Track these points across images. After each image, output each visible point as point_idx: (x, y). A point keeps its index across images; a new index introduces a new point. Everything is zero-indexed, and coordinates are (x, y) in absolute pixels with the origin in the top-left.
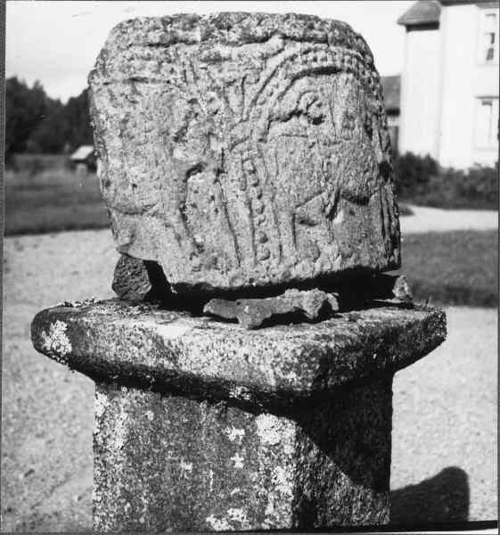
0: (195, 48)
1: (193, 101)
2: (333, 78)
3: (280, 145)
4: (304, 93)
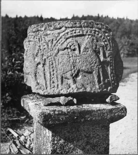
0: (43, 32)
1: (40, 46)
2: (83, 37)
3: (60, 57)
4: (70, 42)
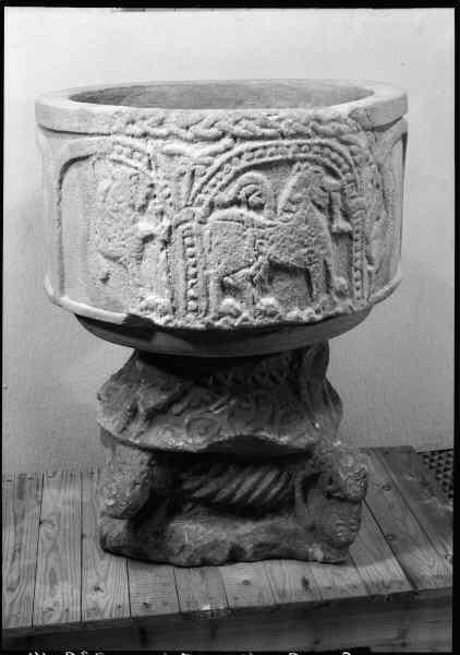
1: (152, 186)
